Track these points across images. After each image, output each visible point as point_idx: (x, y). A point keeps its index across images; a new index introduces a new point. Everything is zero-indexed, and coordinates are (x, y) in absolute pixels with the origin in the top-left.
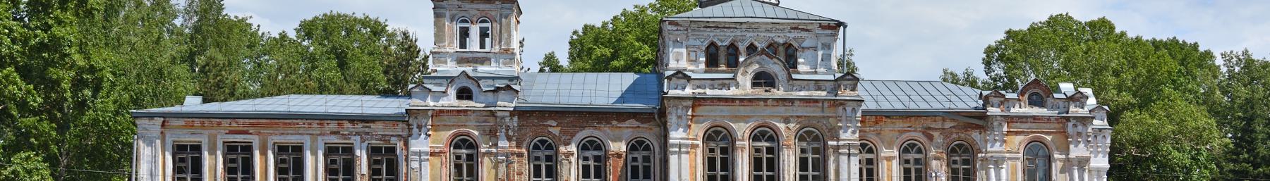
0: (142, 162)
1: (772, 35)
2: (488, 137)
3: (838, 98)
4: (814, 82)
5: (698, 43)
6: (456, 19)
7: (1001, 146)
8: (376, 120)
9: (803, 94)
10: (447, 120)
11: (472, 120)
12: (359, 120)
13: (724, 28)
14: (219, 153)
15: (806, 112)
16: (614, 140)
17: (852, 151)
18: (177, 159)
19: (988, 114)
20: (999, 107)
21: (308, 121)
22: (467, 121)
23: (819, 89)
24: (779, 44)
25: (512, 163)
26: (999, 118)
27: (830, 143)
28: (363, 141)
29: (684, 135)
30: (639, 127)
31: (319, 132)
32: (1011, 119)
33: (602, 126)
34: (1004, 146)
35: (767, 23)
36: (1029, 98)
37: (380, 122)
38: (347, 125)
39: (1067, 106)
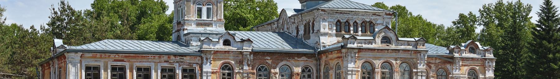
0: (70, 75)
1: (364, 17)
2: (239, 64)
3: (418, 49)
4: (407, 42)
5: (332, 20)
6: (196, 3)
7: (459, 71)
8: (187, 55)
9: (403, 47)
10: (220, 55)
11: (231, 56)
12: (179, 55)
13: (344, 13)
14: (109, 71)
15: (404, 56)
16: (296, 67)
17: (423, 74)
18: (87, 74)
19: (454, 56)
20: (458, 53)
21: (154, 55)
22: (229, 57)
23: (409, 45)
24: (367, 22)
25: (250, 77)
26: (459, 59)
27: (414, 70)
28: (180, 66)
29: (354, 66)
30: (307, 60)
31: (159, 61)
32: (463, 59)
33: (291, 60)
34: (460, 72)
35: (363, 12)
36: (469, 50)
37: (188, 56)
38: (172, 57)
39: (484, 53)
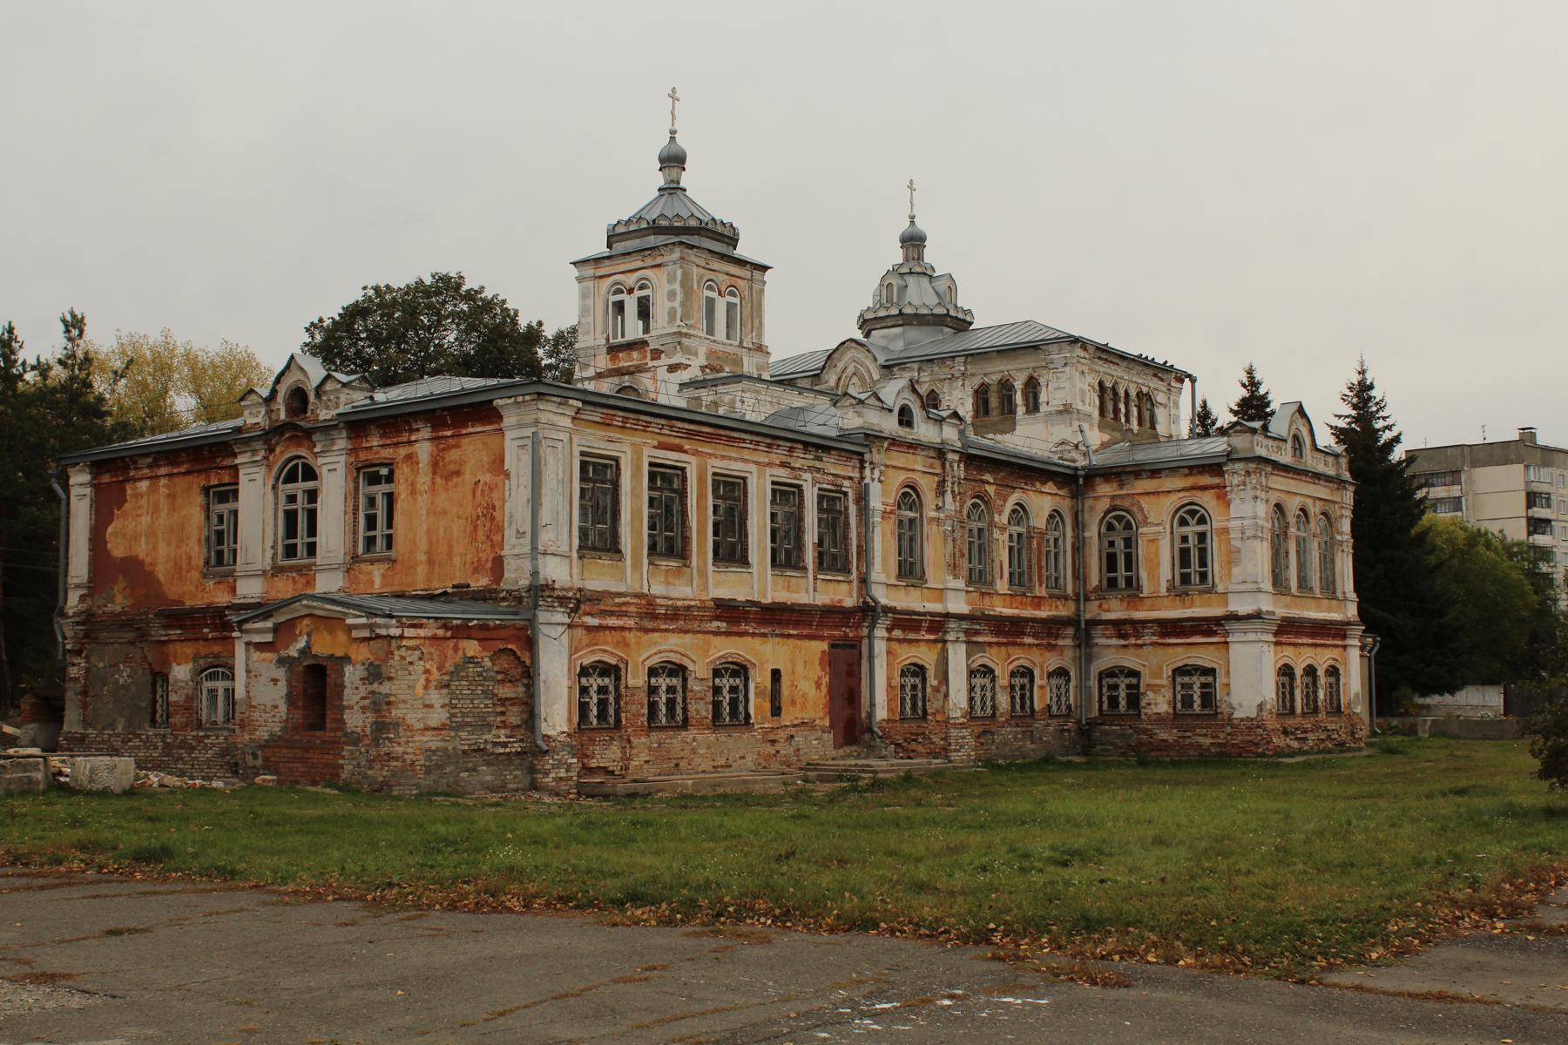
12: (806, 445)
31: (766, 460)
